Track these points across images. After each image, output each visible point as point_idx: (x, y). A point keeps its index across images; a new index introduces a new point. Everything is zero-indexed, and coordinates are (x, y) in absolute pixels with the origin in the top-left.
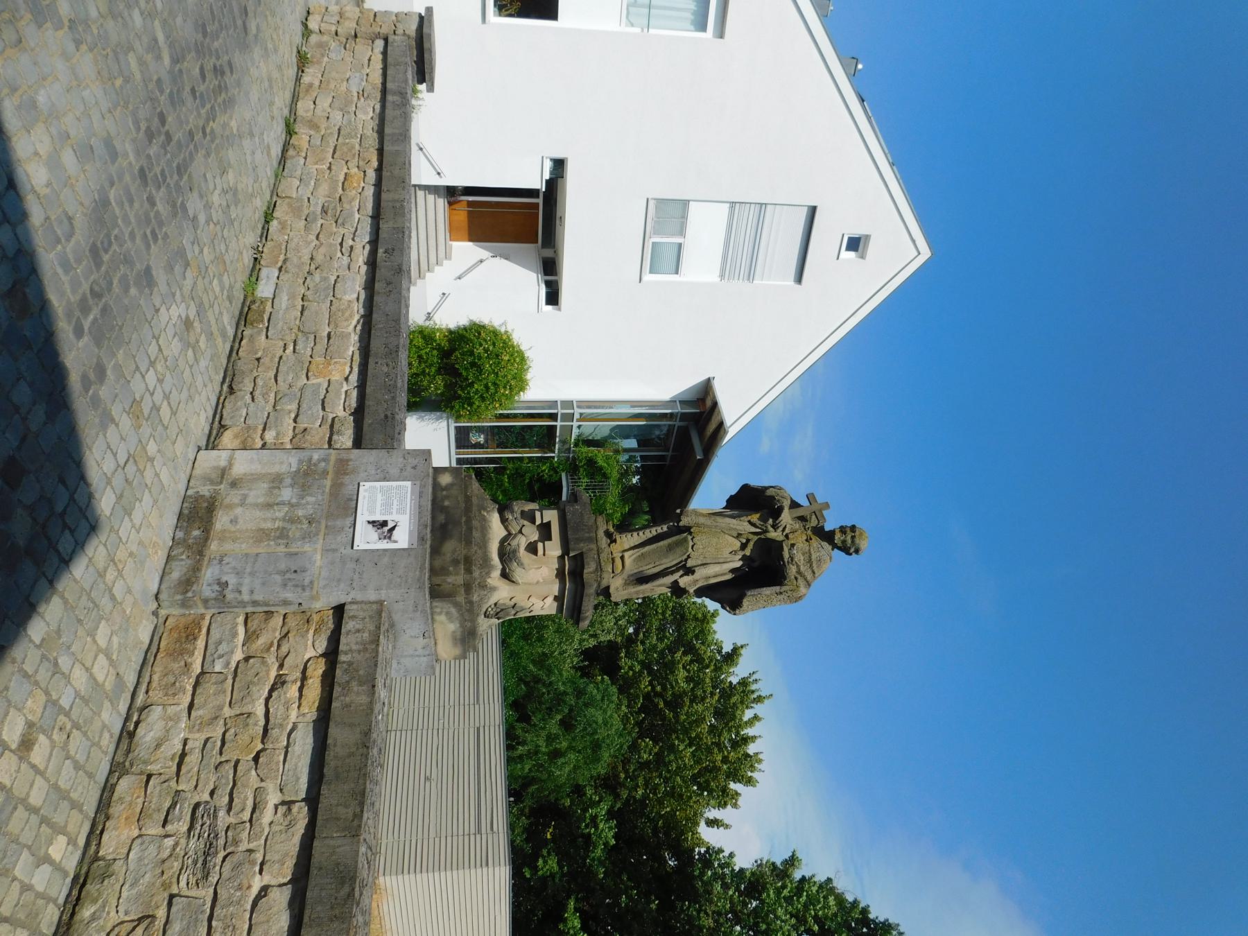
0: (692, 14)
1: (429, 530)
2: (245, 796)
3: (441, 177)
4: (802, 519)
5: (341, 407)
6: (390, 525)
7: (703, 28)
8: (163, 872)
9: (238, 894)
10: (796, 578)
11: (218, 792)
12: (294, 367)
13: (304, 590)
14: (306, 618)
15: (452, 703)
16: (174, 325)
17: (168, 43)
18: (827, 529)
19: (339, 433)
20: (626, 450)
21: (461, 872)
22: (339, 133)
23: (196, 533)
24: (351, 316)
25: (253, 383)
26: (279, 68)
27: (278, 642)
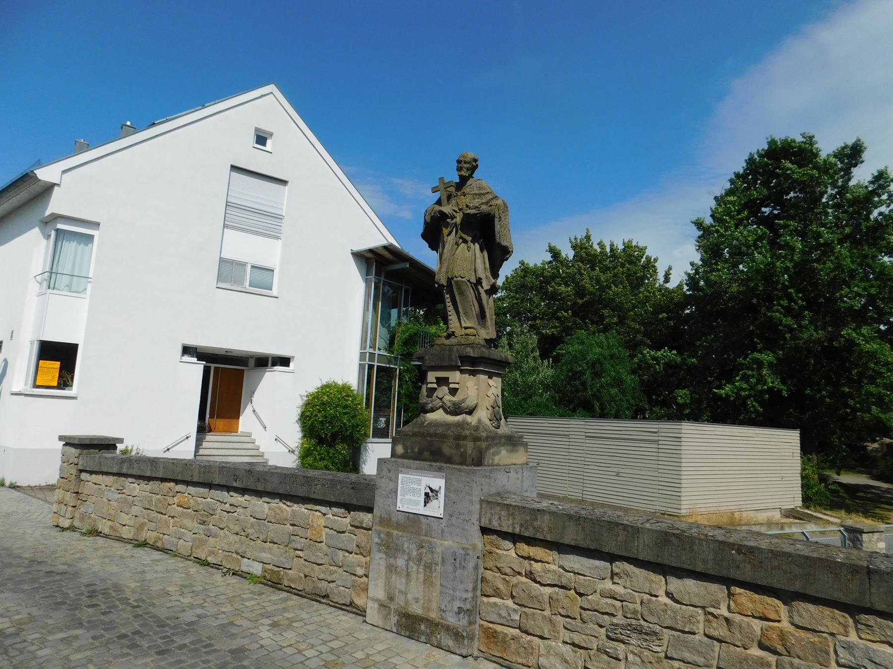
0: (80, 245)
1: (433, 464)
2: (605, 604)
3: (190, 436)
4: (449, 198)
5: (344, 520)
6: (428, 490)
7: (89, 238)
8: (650, 662)
9: (669, 612)
10: (491, 206)
11: (601, 622)
12: (313, 551)
13: (468, 554)
14: (488, 554)
15: (567, 454)
16: (274, 635)
17: (66, 630)
18: (458, 181)
19: (361, 522)
20: (399, 317)
21: (683, 456)
22: (148, 509)
23: (423, 627)
24: (280, 508)
25: (323, 581)
26: (96, 550)
27: (502, 574)
